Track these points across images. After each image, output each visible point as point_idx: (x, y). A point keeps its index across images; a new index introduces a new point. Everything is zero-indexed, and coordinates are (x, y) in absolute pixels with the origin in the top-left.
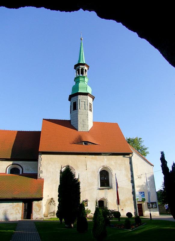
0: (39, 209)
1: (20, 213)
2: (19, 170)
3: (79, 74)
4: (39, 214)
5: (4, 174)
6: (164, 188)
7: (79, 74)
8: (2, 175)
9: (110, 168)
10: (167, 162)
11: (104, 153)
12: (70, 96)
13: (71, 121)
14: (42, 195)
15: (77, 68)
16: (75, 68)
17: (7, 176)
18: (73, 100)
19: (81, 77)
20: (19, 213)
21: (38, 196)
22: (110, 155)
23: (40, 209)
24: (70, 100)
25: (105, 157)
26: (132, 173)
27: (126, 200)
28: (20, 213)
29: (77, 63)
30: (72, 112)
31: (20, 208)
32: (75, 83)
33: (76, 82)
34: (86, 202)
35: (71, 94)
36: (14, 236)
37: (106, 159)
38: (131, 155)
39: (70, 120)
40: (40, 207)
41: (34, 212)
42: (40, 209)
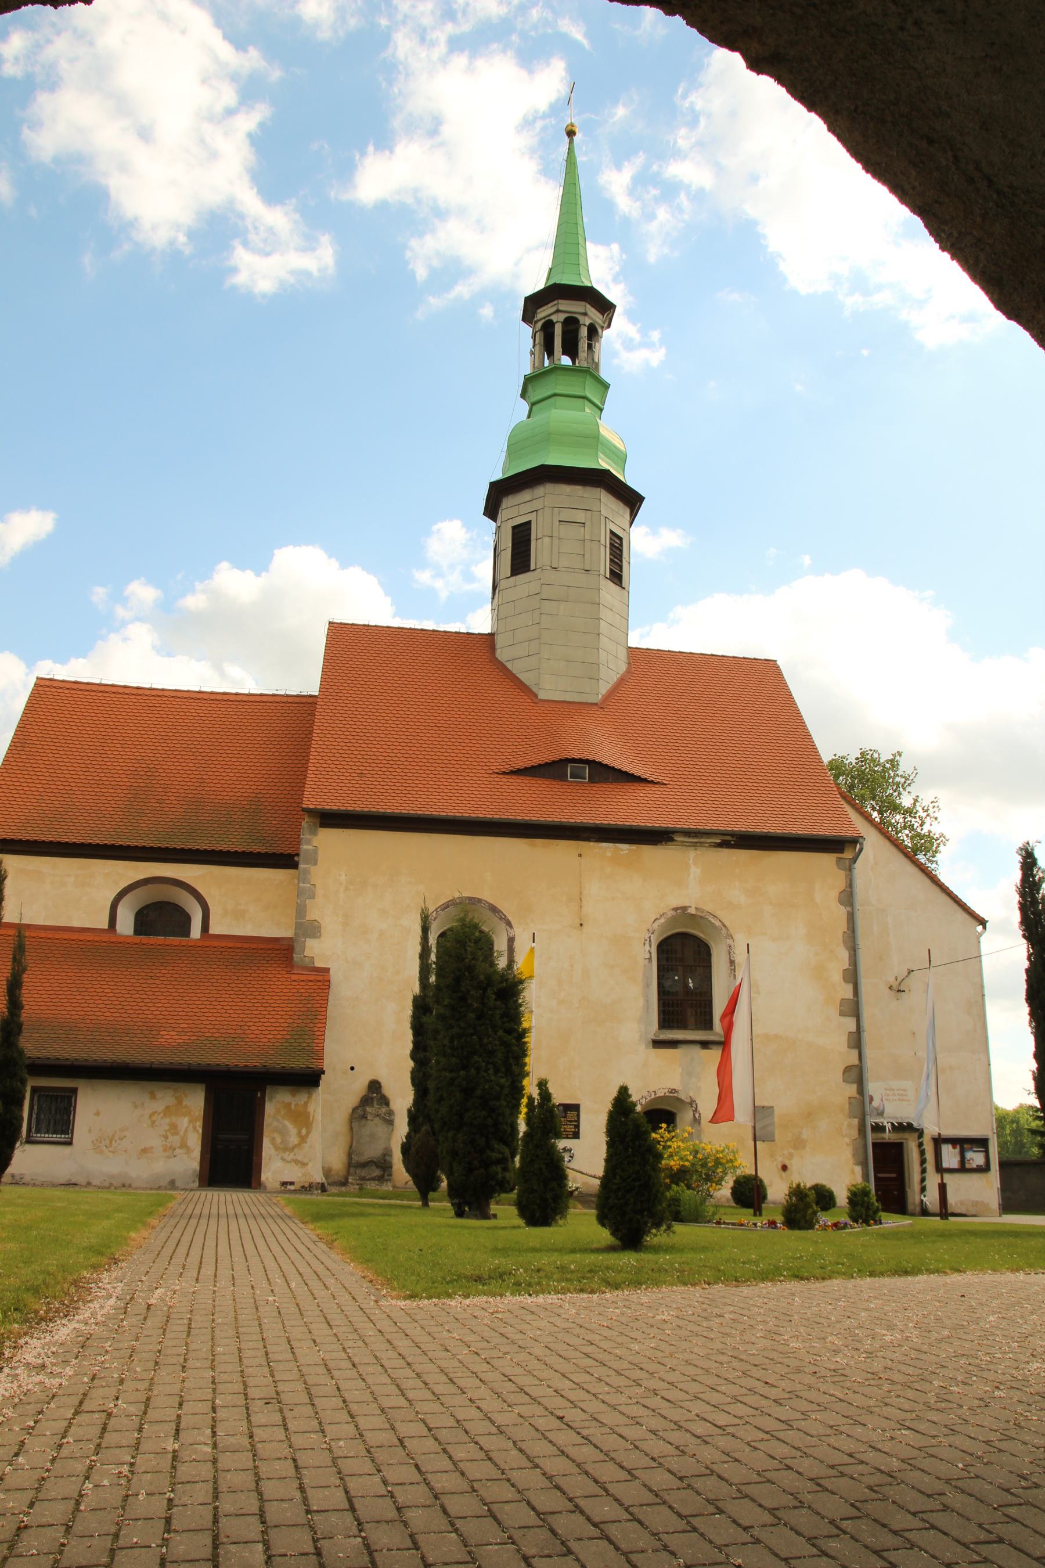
0: (299, 1133)
1: (189, 1151)
2: (187, 919)
3: (549, 348)
4: (296, 1162)
5: (105, 937)
6: (544, 112)
7: (549, 348)
8: (89, 937)
9: (717, 923)
10: (940, 251)
11: (687, 833)
12: (491, 484)
13: (500, 642)
14: (318, 1054)
15: (543, 313)
16: (528, 316)
17: (123, 944)
18: (516, 509)
19: (565, 369)
20: (187, 1147)
21: (298, 1063)
22: (724, 844)
23: (304, 1131)
24: (492, 510)
25: (692, 854)
26: (855, 955)
27: (809, 1115)
28: (189, 1151)
29: (541, 286)
30: (503, 584)
31: (190, 1122)
32: (524, 406)
33: (533, 405)
34: (571, 1115)
35: (498, 475)
36: (572, 1262)
37: (695, 871)
38: (848, 855)
39: (491, 635)
40: (303, 1120)
41: (273, 1152)
42: (304, 1131)
